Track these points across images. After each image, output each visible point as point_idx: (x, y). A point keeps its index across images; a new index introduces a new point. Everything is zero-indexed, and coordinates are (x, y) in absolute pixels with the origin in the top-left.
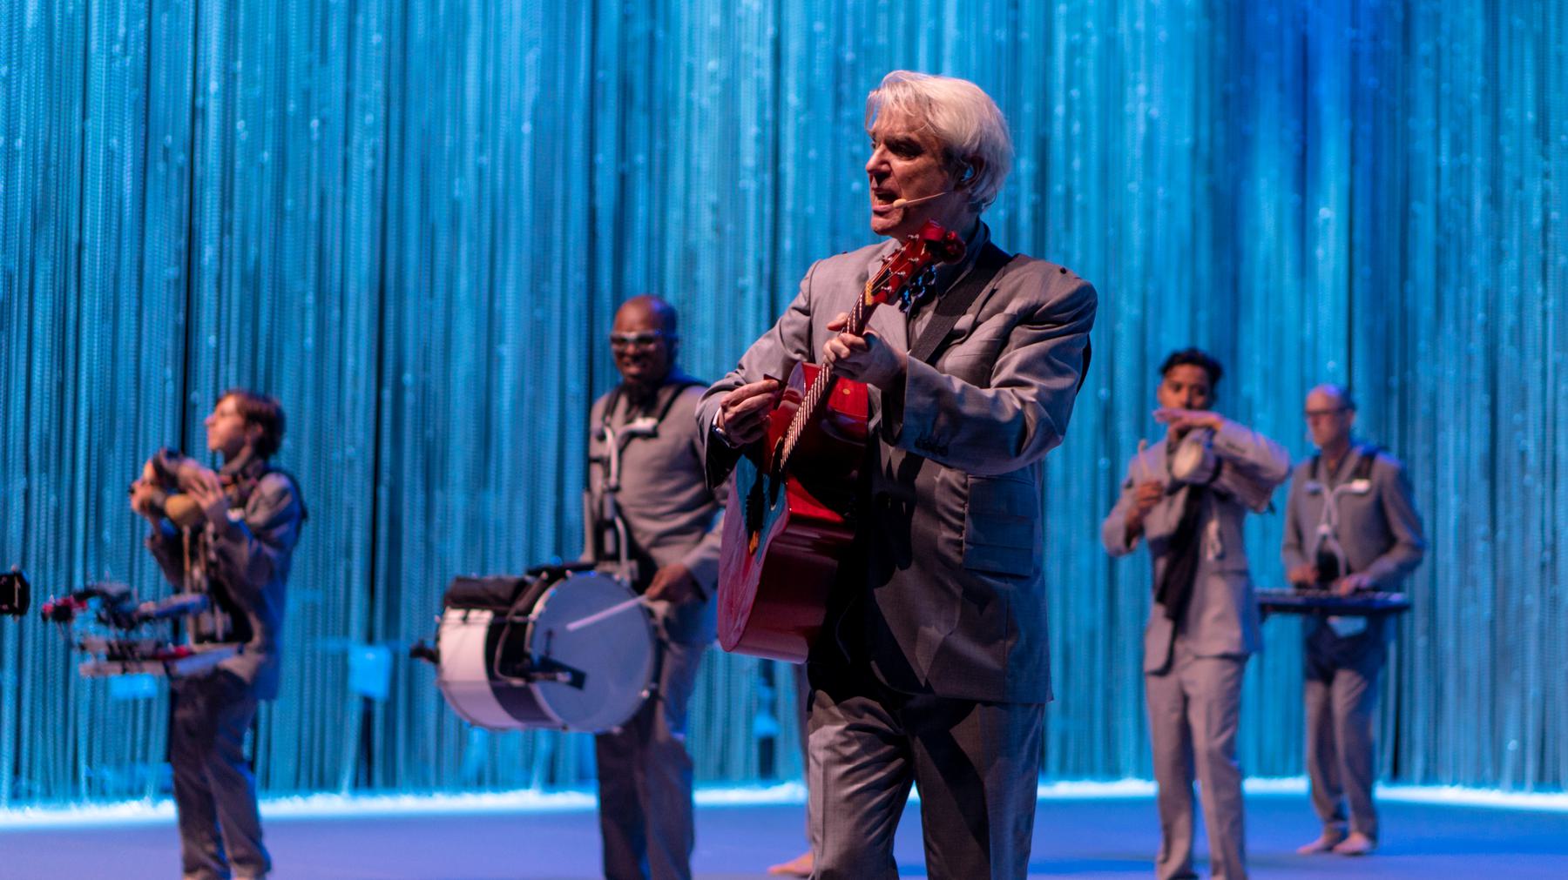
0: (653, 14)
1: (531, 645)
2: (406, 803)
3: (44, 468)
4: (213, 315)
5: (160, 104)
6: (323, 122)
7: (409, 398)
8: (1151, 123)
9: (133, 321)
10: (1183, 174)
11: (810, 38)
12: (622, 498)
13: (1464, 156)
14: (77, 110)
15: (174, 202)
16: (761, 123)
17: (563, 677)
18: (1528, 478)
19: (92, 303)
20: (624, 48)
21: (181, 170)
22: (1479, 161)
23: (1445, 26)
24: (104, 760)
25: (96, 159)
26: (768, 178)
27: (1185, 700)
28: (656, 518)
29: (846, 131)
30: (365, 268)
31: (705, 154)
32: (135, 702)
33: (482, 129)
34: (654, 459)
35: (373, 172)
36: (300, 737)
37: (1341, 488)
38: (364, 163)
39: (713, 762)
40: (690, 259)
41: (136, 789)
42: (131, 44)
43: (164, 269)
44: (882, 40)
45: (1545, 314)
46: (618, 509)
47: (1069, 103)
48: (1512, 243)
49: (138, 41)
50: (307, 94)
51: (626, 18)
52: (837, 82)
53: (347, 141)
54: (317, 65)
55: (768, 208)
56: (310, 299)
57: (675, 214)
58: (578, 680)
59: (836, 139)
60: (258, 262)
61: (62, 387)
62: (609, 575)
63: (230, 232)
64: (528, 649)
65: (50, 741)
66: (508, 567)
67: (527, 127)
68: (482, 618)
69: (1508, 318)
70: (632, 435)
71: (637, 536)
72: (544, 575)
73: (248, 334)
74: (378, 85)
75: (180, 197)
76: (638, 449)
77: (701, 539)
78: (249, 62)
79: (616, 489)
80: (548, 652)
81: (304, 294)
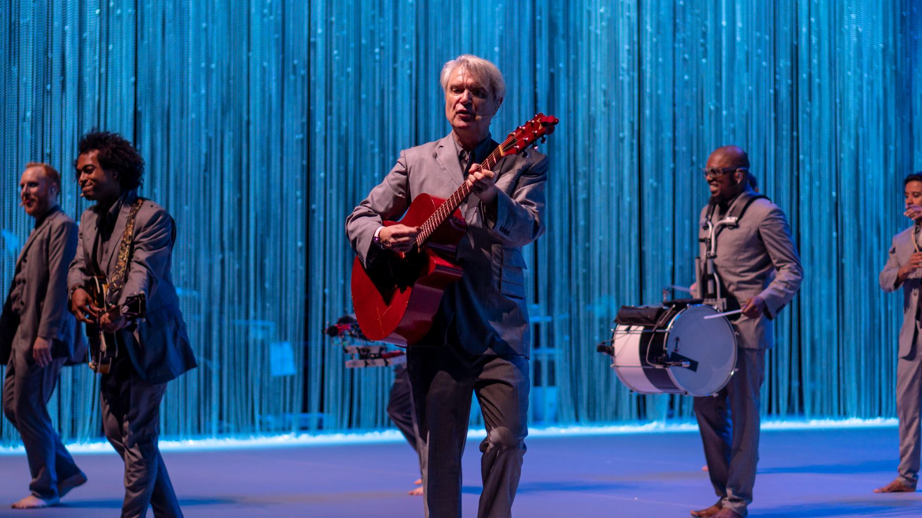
3: (232, 249)
5: (290, 43)
6: (382, 48)
8: (859, 35)
9: (278, 164)
12: (716, 261)
14: (245, 47)
15: (300, 97)
16: (631, 43)
17: (686, 364)
19: (256, 155)
21: (303, 77)
24: (269, 412)
25: (256, 74)
28: (735, 274)
30: (407, 133)
31: (599, 65)
32: (285, 378)
34: (736, 240)
35: (411, 76)
36: (377, 400)
38: (405, 72)
39: (611, 409)
40: (591, 122)
41: (287, 427)
42: (274, 9)
43: (295, 135)
46: (715, 267)
49: (277, 8)
50: (372, 33)
53: (395, 60)
54: (377, 17)
57: (582, 97)
58: (694, 366)
60: (347, 128)
61: (240, 201)
62: (711, 306)
64: (665, 348)
65: (238, 403)
66: (654, 300)
70: (724, 226)
71: (726, 284)
75: (303, 94)
78: (339, 19)
80: (676, 350)
81: (373, 147)
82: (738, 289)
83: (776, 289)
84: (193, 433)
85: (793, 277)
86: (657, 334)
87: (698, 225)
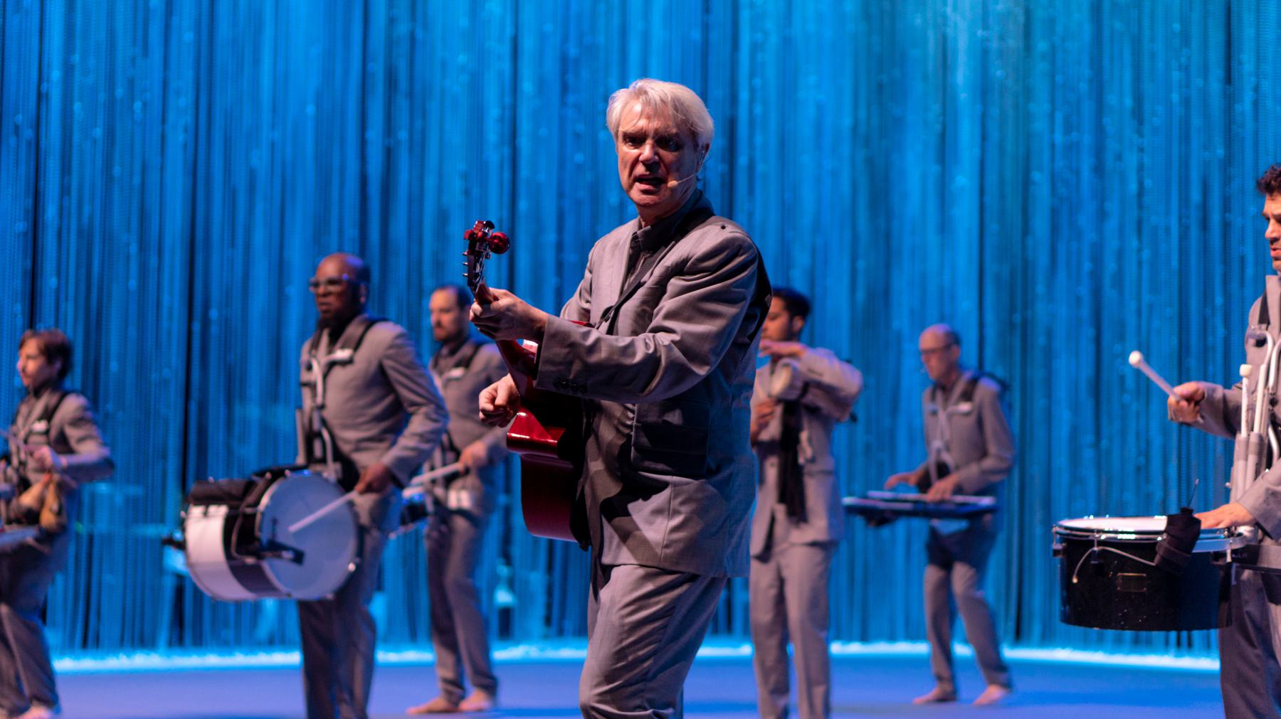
0: (413, 17)
1: (260, 530)
2: (212, 660)
4: (54, 262)
6: (145, 105)
7: (214, 329)
8: (820, 108)
10: (846, 149)
11: (542, 38)
12: (327, 413)
13: (1074, 134)
17: (288, 555)
18: (1127, 398)
20: (390, 44)
21: (29, 143)
22: (1087, 139)
23: (1059, 29)
26: (506, 151)
27: (781, 582)
29: (570, 112)
31: (456, 133)
33: (274, 110)
35: (185, 146)
36: (124, 608)
37: (951, 409)
38: (178, 138)
44: (601, 39)
45: (1140, 264)
46: (324, 422)
47: (752, 91)
48: (1112, 206)
50: (131, 83)
51: (392, 21)
52: (564, 72)
55: (507, 175)
56: (134, 249)
57: (431, 181)
58: (299, 557)
59: (562, 120)
60: (91, 218)
62: (319, 474)
63: (69, 194)
64: (257, 533)
67: (311, 109)
68: (219, 513)
69: (1110, 266)
70: (332, 365)
72: (268, 475)
73: (83, 278)
74: (189, 74)
76: (339, 374)
77: (393, 443)
79: (322, 407)
80: (274, 535)
81: (128, 245)
82: (357, 450)
83: (407, 448)
84: (170, 644)
85: (430, 426)
86: (246, 516)
87: (298, 365)
